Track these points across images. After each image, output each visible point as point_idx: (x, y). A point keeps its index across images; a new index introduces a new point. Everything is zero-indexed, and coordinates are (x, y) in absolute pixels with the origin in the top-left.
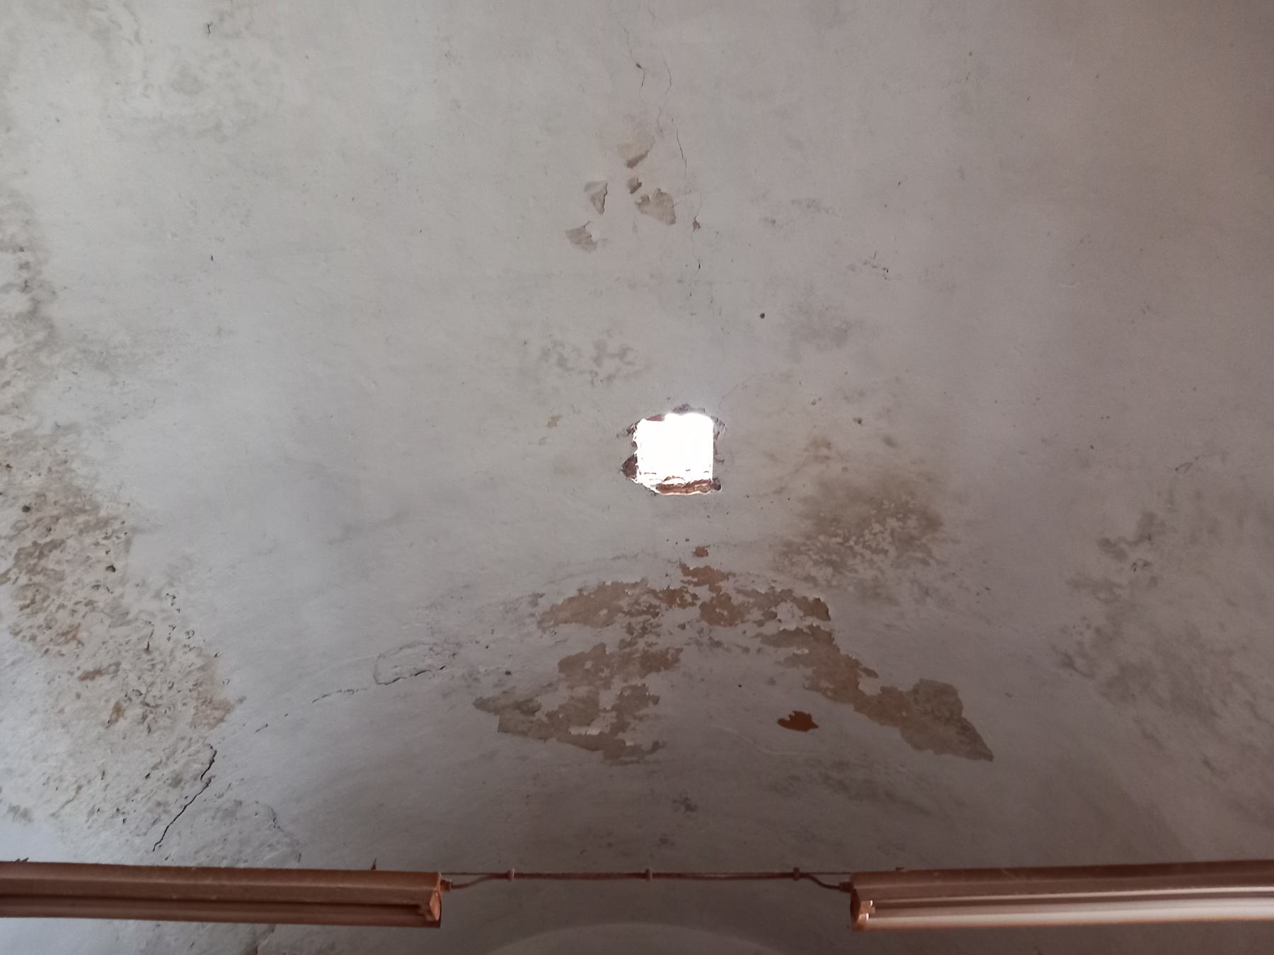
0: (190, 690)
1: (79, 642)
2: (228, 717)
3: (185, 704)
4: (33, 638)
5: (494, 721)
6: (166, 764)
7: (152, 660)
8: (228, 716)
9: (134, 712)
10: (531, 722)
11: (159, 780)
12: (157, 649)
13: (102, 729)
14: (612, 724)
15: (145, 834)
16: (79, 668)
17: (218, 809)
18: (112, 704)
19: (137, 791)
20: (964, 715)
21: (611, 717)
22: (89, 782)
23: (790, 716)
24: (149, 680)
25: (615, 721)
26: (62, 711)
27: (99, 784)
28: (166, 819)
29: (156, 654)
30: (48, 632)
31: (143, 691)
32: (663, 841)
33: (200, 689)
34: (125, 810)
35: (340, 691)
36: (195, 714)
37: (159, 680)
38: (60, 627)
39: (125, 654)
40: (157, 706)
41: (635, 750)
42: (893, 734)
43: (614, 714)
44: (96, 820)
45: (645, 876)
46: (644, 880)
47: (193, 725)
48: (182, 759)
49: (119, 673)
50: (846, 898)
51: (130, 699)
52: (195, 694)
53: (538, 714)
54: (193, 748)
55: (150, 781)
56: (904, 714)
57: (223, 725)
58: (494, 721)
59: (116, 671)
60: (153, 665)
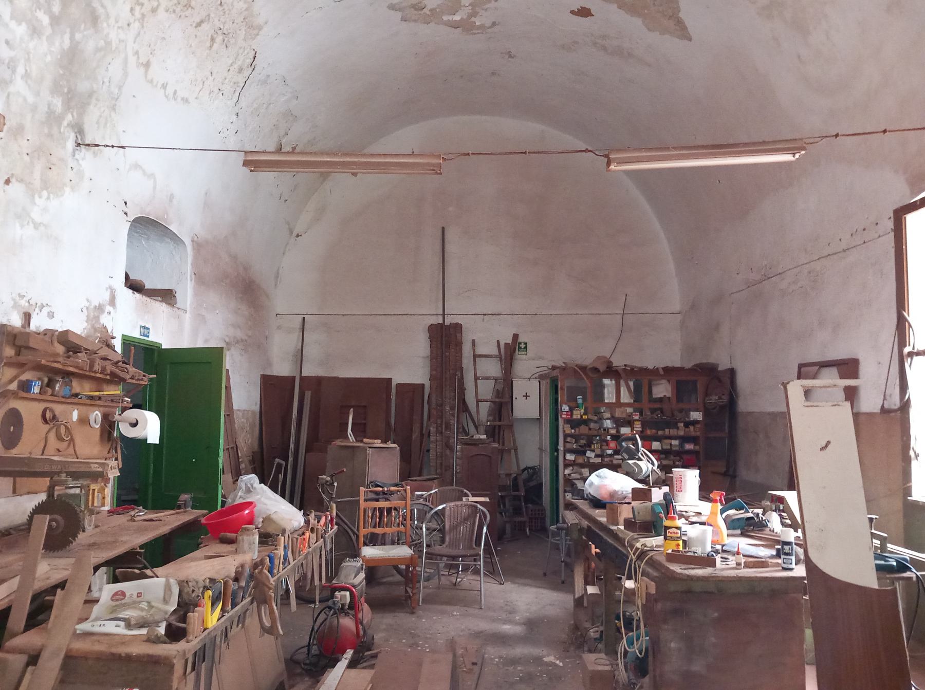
0: (242, 22)
1: (192, 8)
2: (261, 33)
3: (240, 30)
4: (174, 11)
5: (399, 15)
6: (236, 63)
7: (224, 9)
8: (260, 32)
9: (219, 39)
10: (420, 14)
11: (233, 71)
12: (225, 3)
13: (208, 51)
14: (468, 13)
15: (232, 99)
16: (194, 22)
17: (259, 81)
18: (210, 37)
19: (226, 79)
20: (681, 15)
21: (469, 10)
22: (207, 79)
23: (578, 9)
24: (223, 21)
25: (470, 11)
26: (191, 46)
27: (211, 78)
28: (239, 90)
29: (225, 7)
30: (179, 6)
31: (222, 27)
32: (493, 74)
33: (247, 20)
34: (223, 89)
35: (315, 9)
36: (245, 34)
37: (228, 20)
38: (184, 2)
39: (211, 9)
40: (229, 33)
41: (482, 27)
42: (637, 22)
43: (470, 8)
44: (212, 97)
45: (525, 153)
46: (524, 155)
47: (245, 40)
48: (241, 58)
49: (210, 20)
50: (606, 159)
51: (217, 33)
52: (244, 23)
53: (425, 11)
54: (246, 52)
55: (230, 73)
56: (646, 11)
57: (258, 37)
58: (399, 15)
59: (209, 19)
60: (224, 12)
